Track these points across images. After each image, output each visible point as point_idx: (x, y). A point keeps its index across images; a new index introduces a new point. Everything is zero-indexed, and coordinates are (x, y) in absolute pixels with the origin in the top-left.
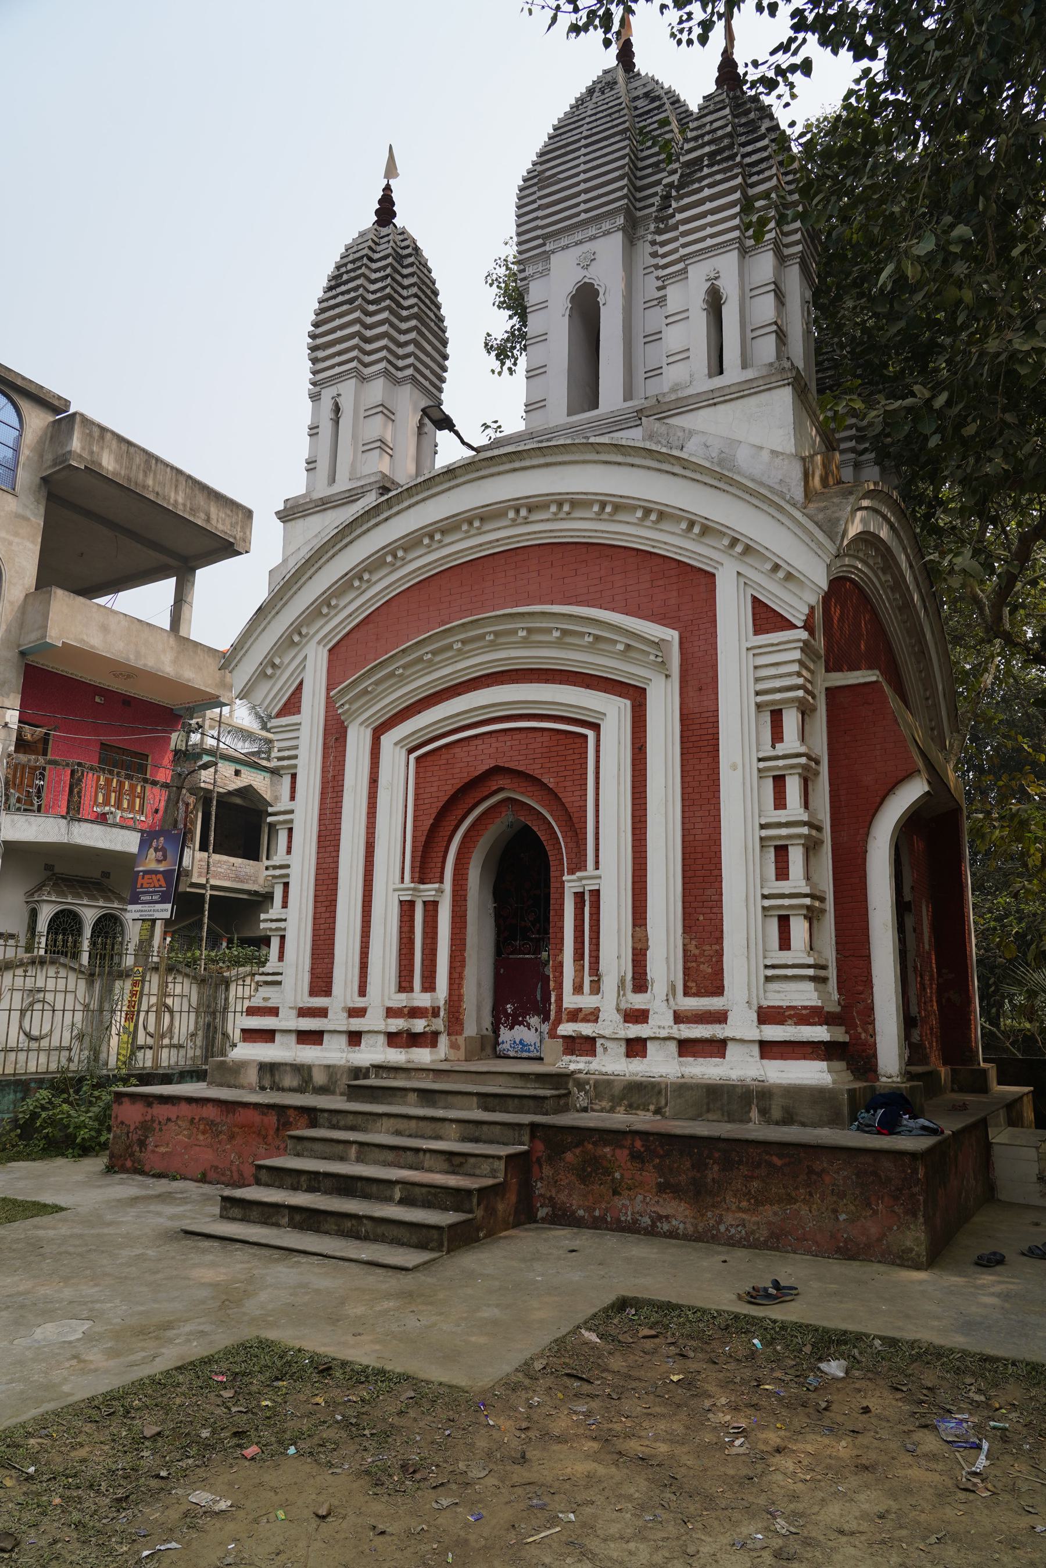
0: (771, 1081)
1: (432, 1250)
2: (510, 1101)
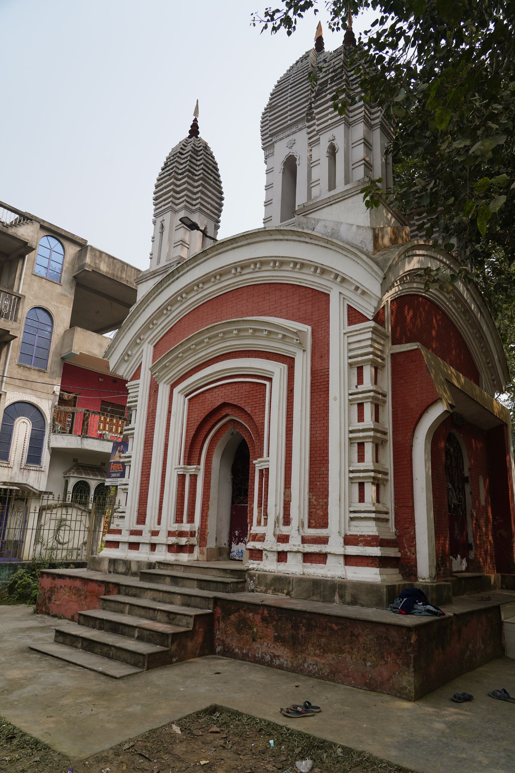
0: (349, 579)
1: (140, 667)
2: (211, 584)
